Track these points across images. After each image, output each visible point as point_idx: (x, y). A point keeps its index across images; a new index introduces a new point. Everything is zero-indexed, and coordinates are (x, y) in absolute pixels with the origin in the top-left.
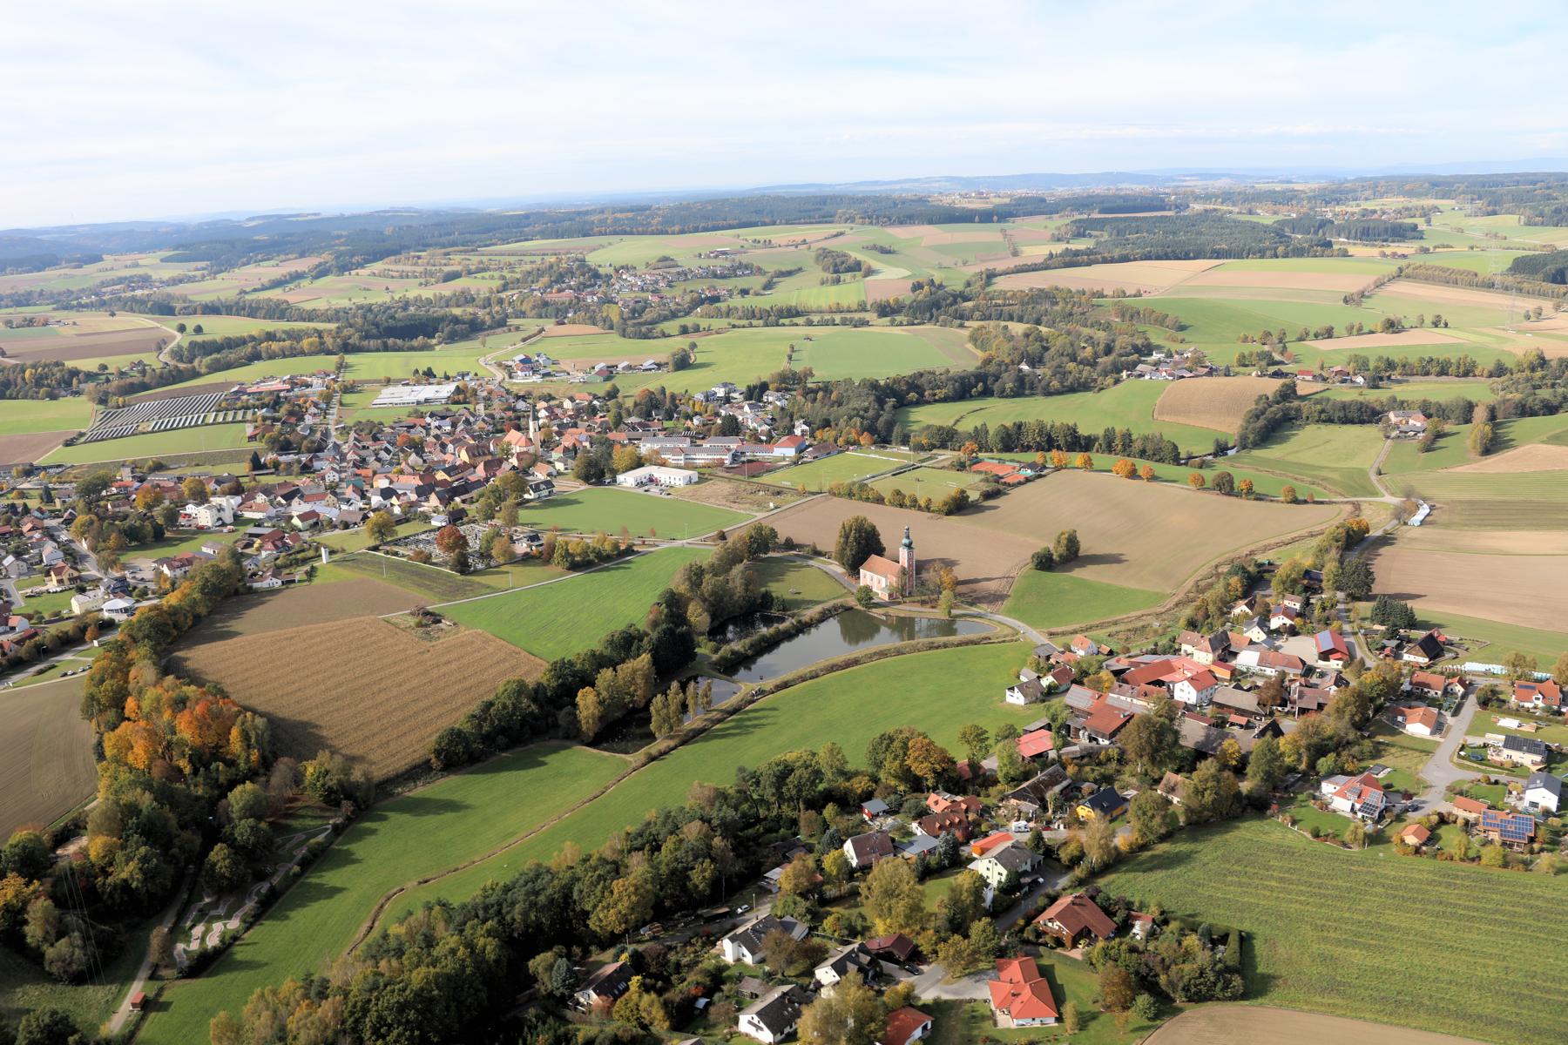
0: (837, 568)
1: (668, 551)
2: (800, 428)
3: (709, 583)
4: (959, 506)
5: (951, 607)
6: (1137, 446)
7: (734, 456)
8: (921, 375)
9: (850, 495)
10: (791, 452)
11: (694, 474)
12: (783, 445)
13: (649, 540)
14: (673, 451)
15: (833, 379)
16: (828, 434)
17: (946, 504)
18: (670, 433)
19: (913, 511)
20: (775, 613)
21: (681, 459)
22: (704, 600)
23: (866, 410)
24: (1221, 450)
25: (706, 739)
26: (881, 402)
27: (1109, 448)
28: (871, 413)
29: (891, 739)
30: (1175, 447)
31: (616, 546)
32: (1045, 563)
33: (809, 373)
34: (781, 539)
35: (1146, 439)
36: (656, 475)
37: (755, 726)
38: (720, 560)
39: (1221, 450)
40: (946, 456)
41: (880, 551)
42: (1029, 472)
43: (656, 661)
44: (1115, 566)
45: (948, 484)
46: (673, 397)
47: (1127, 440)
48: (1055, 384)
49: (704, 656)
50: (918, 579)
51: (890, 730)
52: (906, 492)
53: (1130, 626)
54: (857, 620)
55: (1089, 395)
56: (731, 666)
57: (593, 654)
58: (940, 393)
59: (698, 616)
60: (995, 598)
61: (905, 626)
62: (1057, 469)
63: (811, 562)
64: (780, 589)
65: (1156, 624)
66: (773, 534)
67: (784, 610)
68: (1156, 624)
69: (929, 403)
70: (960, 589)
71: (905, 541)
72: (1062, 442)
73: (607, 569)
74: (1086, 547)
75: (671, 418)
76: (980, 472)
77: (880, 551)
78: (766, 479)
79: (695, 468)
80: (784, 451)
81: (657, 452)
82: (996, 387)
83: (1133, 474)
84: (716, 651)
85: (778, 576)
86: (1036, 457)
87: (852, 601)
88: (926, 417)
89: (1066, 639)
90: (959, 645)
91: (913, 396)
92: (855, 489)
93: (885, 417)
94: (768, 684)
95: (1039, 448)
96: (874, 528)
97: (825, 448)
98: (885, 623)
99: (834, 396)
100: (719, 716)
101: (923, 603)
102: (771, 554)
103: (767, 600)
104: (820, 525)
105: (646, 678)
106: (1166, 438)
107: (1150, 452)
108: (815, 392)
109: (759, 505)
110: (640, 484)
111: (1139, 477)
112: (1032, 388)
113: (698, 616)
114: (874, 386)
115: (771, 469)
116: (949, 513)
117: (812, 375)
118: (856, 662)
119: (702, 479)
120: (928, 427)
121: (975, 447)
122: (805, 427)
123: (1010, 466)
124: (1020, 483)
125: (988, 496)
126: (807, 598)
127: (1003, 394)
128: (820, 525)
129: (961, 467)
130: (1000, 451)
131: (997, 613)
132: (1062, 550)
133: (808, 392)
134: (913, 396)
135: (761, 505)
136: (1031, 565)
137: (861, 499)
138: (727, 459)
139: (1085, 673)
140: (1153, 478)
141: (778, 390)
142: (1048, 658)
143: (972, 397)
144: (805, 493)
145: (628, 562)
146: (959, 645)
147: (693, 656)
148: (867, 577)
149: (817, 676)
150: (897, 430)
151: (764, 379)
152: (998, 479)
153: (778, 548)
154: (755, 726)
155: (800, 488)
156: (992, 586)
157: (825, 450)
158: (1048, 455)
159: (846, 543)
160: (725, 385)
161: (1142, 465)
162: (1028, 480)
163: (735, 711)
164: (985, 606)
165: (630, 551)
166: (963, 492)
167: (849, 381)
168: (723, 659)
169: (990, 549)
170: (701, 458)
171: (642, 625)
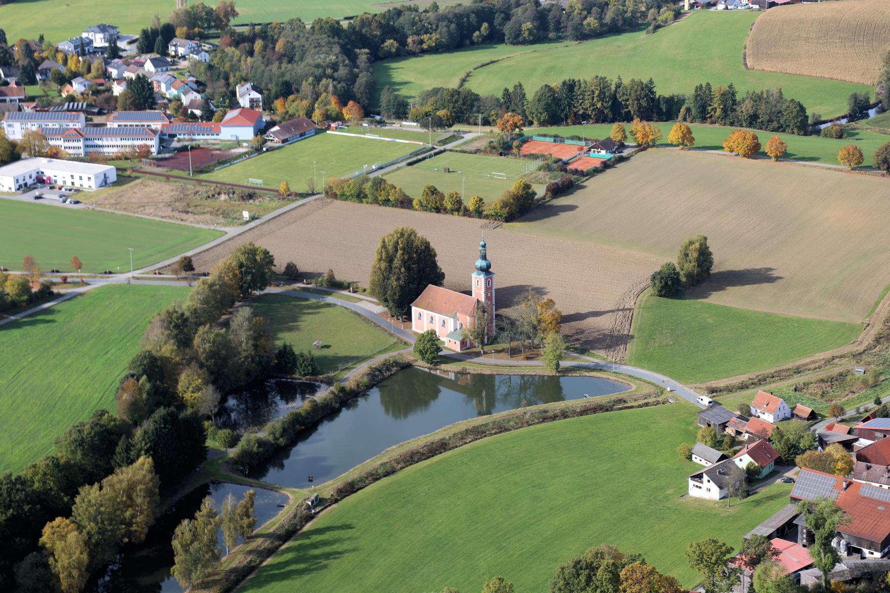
0: (372, 307)
1: (109, 291)
2: (246, 96)
3: (203, 339)
4: (523, 208)
5: (560, 357)
6: (745, 109)
7: (161, 141)
8: (399, 13)
9: (360, 196)
10: (247, 133)
11: (109, 169)
12: (232, 123)
13: (73, 275)
14: (63, 133)
15: (275, 20)
16: (296, 105)
17: (505, 205)
18: (44, 106)
19: (457, 220)
20: (299, 377)
21: (78, 146)
22: (201, 365)
23: (335, 67)
24: (860, 109)
25: (259, 583)
26: (349, 53)
27: (704, 115)
28: (342, 72)
29: (592, 568)
30: (802, 109)
31: (24, 287)
32: (671, 286)
33: (231, 12)
34: (280, 266)
35: (758, 98)
36: (48, 173)
37: (327, 556)
38: (206, 301)
39: (860, 109)
40: (474, 134)
41: (437, 278)
42: (604, 154)
43: (158, 467)
44: (765, 286)
45: (503, 178)
46: (28, 49)
47: (729, 99)
48: (591, 21)
49: (216, 451)
50: (501, 318)
51: (587, 555)
52: (446, 188)
53: (823, 374)
54: (406, 384)
55: (641, 36)
56: (260, 463)
57: (55, 463)
58: (430, 40)
59: (193, 389)
60: (613, 341)
61: (482, 389)
62: (641, 148)
63: (330, 299)
64: (305, 338)
65: (859, 370)
66: (269, 259)
67: (315, 373)
68: (859, 370)
69: (413, 54)
70: (566, 328)
71: (480, 263)
72: (632, 109)
73: (16, 325)
74: (724, 260)
75: (33, 82)
76: (534, 157)
77: (437, 278)
78: (221, 174)
79: (106, 160)
80: (235, 132)
81: (43, 135)
82: (507, 29)
83: (755, 152)
84: (233, 442)
85: (290, 322)
86: (611, 131)
87: (409, 355)
88: (420, 76)
89: (739, 397)
90: (585, 412)
91: (390, 44)
92: (367, 186)
93: (363, 79)
94: (328, 489)
95: (602, 118)
96: (427, 245)
97: (297, 125)
98: (452, 385)
99: (279, 46)
100: (267, 544)
101: (514, 352)
102: (271, 290)
103: (287, 359)
104: (346, 245)
105: (149, 493)
106: (787, 96)
107: (763, 118)
108: (251, 39)
109: (225, 215)
110: (24, 188)
111: (764, 155)
112: (558, 29)
113: (193, 389)
114: (335, 30)
115: (224, 160)
116: (510, 218)
117: (235, 14)
118: (443, 446)
119: (122, 179)
120: (436, 91)
121: (518, 118)
122: (256, 95)
123: (574, 145)
124: (596, 171)
125: (559, 190)
126: (342, 353)
127: (518, 40)
128: (346, 245)
129: (505, 149)
130: (543, 124)
131: (622, 362)
132: (691, 266)
133: (238, 40)
134: (390, 44)
135: (229, 216)
136: (650, 291)
137: (376, 201)
138: (153, 144)
139: (794, 449)
140: (784, 156)
141: (189, 37)
142: (724, 426)
143: (473, 45)
144: (290, 196)
145: (49, 311)
146: (585, 412)
147: (202, 452)
148: (424, 319)
149: (393, 472)
150: (384, 98)
151: (164, 21)
152: (563, 166)
153: (278, 279)
154: (327, 556)
155: (282, 188)
156: (605, 323)
157: (299, 129)
158: (628, 127)
159: (390, 268)
160: (103, 29)
161: (768, 139)
162: (606, 165)
163: (289, 534)
164: (602, 353)
165: (47, 294)
166: (527, 186)
167: (297, 24)
168: (246, 454)
169: (588, 265)
170: (112, 145)
171: (117, 412)
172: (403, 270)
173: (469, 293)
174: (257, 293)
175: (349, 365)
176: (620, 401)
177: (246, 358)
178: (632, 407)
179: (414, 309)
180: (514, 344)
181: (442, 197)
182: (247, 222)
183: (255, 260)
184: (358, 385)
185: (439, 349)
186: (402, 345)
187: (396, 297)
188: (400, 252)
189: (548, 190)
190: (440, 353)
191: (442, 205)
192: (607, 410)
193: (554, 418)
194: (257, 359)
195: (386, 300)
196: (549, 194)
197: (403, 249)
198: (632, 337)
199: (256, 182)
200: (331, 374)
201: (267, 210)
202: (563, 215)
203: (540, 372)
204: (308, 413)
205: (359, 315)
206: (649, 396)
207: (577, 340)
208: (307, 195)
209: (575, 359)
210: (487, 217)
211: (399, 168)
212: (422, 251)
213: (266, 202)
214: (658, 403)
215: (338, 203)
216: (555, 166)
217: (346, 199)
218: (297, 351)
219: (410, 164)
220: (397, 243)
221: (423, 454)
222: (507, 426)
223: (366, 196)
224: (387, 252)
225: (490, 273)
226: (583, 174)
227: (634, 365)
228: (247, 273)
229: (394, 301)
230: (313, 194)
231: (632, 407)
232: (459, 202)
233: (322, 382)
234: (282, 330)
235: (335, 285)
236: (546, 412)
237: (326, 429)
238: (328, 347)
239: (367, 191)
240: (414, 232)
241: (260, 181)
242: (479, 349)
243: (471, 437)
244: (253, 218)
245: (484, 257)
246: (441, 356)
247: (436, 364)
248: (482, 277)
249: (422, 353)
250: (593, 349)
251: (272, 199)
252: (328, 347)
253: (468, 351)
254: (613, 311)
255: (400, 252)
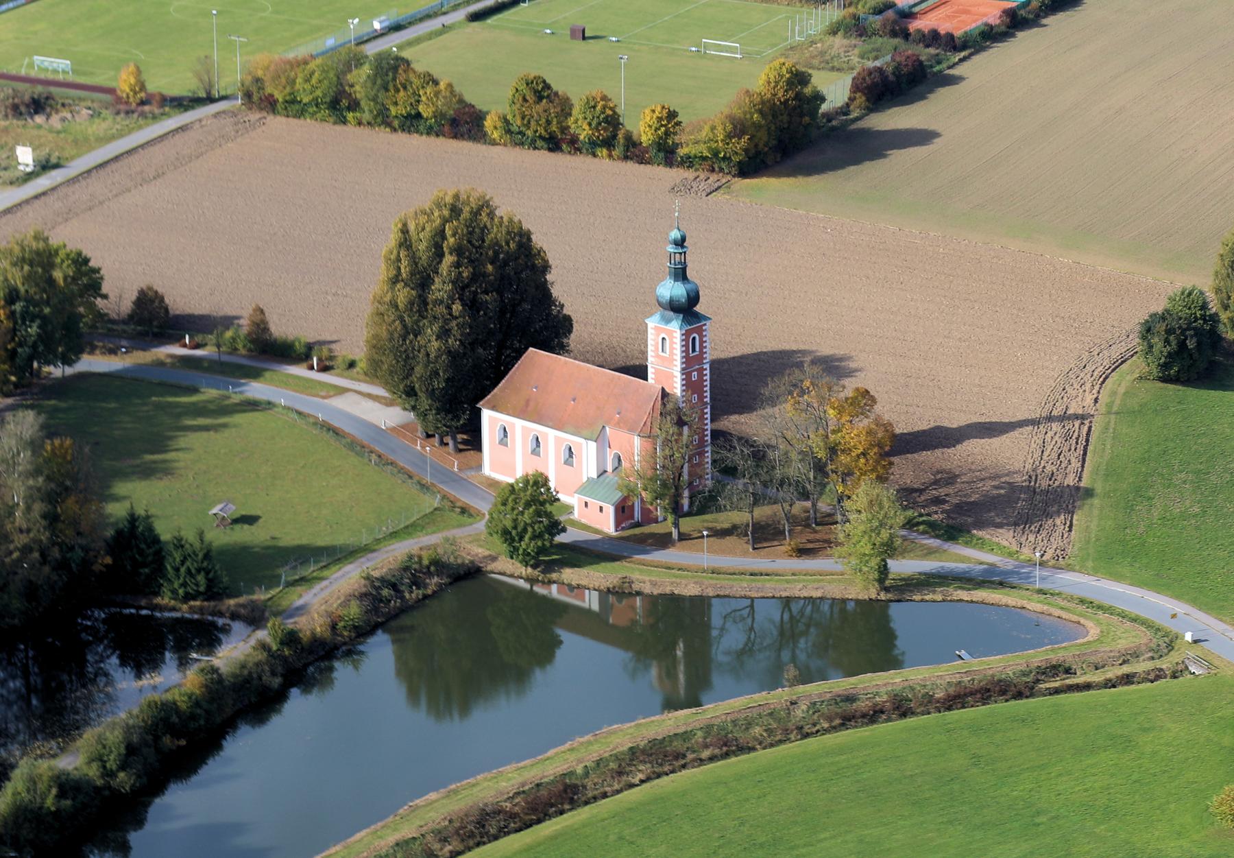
0: (373, 410)
5: (889, 549)
9: (339, 105)
17: (738, 128)
20: (171, 604)
41: (552, 332)
60: (1035, 504)
63: (256, 389)
67: (214, 592)
70: (906, 469)
71: (670, 289)
77: (552, 332)
85: (147, 450)
87: (474, 542)
92: (360, 78)
96: (524, 238)
101: (763, 535)
102: (94, 363)
118: (565, 795)
125: (885, 89)
126: (290, 537)
136: (1138, 365)
137: (383, 119)
144: (146, 103)
148: (514, 444)
153: (112, 332)
155: (124, 83)
156: (1013, 455)
159: (421, 304)
164: (1005, 537)
172: (457, 308)
173: (640, 372)
174: (56, 371)
175: (309, 570)
176: (1054, 669)
177: (26, 550)
178: (1087, 687)
179: (487, 415)
180: (763, 512)
181: (565, 108)
182: (29, 177)
183: (51, 281)
184: (334, 627)
185: (555, 527)
186: (455, 516)
187: (439, 384)
188: (449, 259)
189: (856, 88)
190: (560, 538)
191: (564, 129)
192: (1019, 695)
193: (874, 716)
194: (56, 553)
195: (410, 392)
196: (861, 99)
197: (458, 251)
198: (1089, 493)
199: (54, 65)
200: (260, 596)
201: (83, 144)
202: (900, 158)
203: (835, 590)
204: (197, 704)
205: (336, 432)
206: (1136, 655)
207: (937, 501)
208: (195, 102)
209: (929, 553)
210: (688, 162)
211: (445, 29)
212: (511, 257)
213: (82, 121)
214: (1159, 675)
215: (277, 123)
216: (876, 21)
217: (300, 114)
218: (165, 531)
219: (477, 17)
220: (441, 233)
221: (513, 816)
222: (743, 738)
223: (354, 106)
224: (414, 260)
225: (698, 317)
226: (952, 44)
227: (1095, 572)
228: (27, 317)
229: (431, 394)
230: (210, 100)
231: (1087, 687)
232: (612, 121)
233: (235, 616)
234: (124, 475)
235: (270, 350)
236: (850, 699)
237: (245, 748)
238: (250, 520)
239: (359, 92)
240: (487, 204)
241: (63, 64)
242: (666, 526)
243: (645, 769)
244: (45, 166)
245: (681, 274)
246: (563, 546)
247: (550, 567)
248: (675, 329)
249: (510, 537)
250: (981, 525)
251: (95, 115)
252: (250, 520)
253: (636, 533)
254: (1034, 422)
255: (449, 259)
